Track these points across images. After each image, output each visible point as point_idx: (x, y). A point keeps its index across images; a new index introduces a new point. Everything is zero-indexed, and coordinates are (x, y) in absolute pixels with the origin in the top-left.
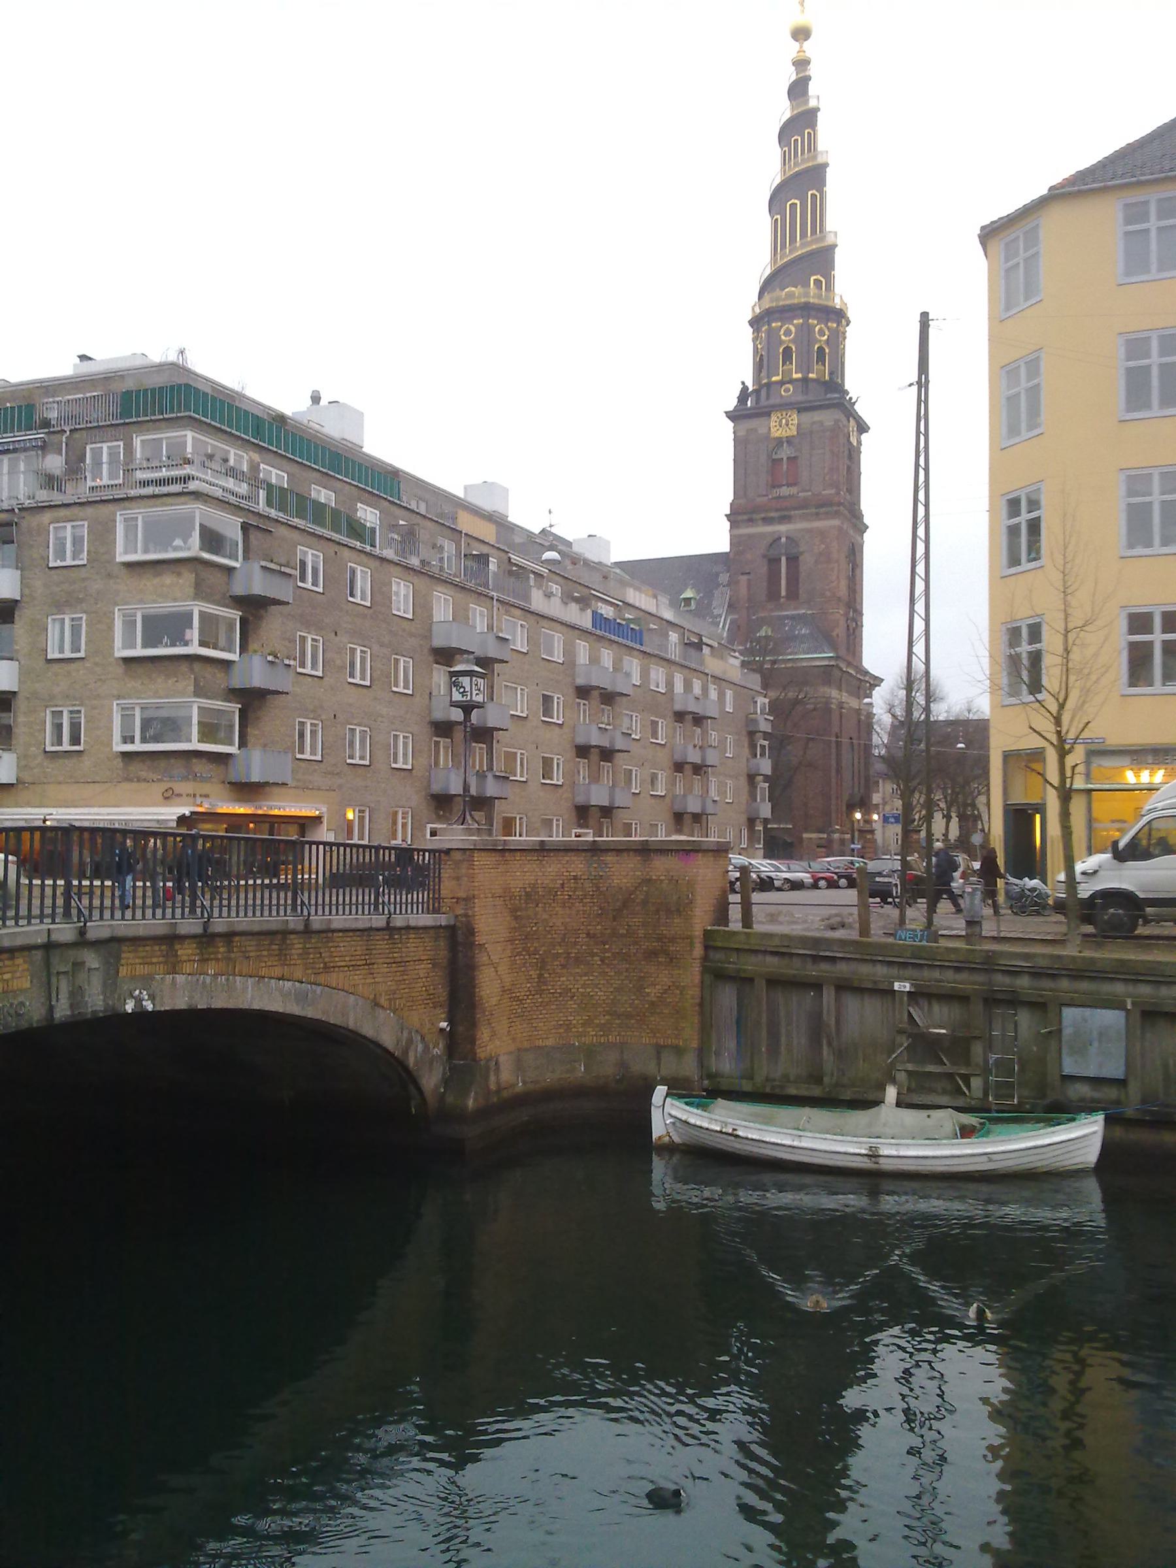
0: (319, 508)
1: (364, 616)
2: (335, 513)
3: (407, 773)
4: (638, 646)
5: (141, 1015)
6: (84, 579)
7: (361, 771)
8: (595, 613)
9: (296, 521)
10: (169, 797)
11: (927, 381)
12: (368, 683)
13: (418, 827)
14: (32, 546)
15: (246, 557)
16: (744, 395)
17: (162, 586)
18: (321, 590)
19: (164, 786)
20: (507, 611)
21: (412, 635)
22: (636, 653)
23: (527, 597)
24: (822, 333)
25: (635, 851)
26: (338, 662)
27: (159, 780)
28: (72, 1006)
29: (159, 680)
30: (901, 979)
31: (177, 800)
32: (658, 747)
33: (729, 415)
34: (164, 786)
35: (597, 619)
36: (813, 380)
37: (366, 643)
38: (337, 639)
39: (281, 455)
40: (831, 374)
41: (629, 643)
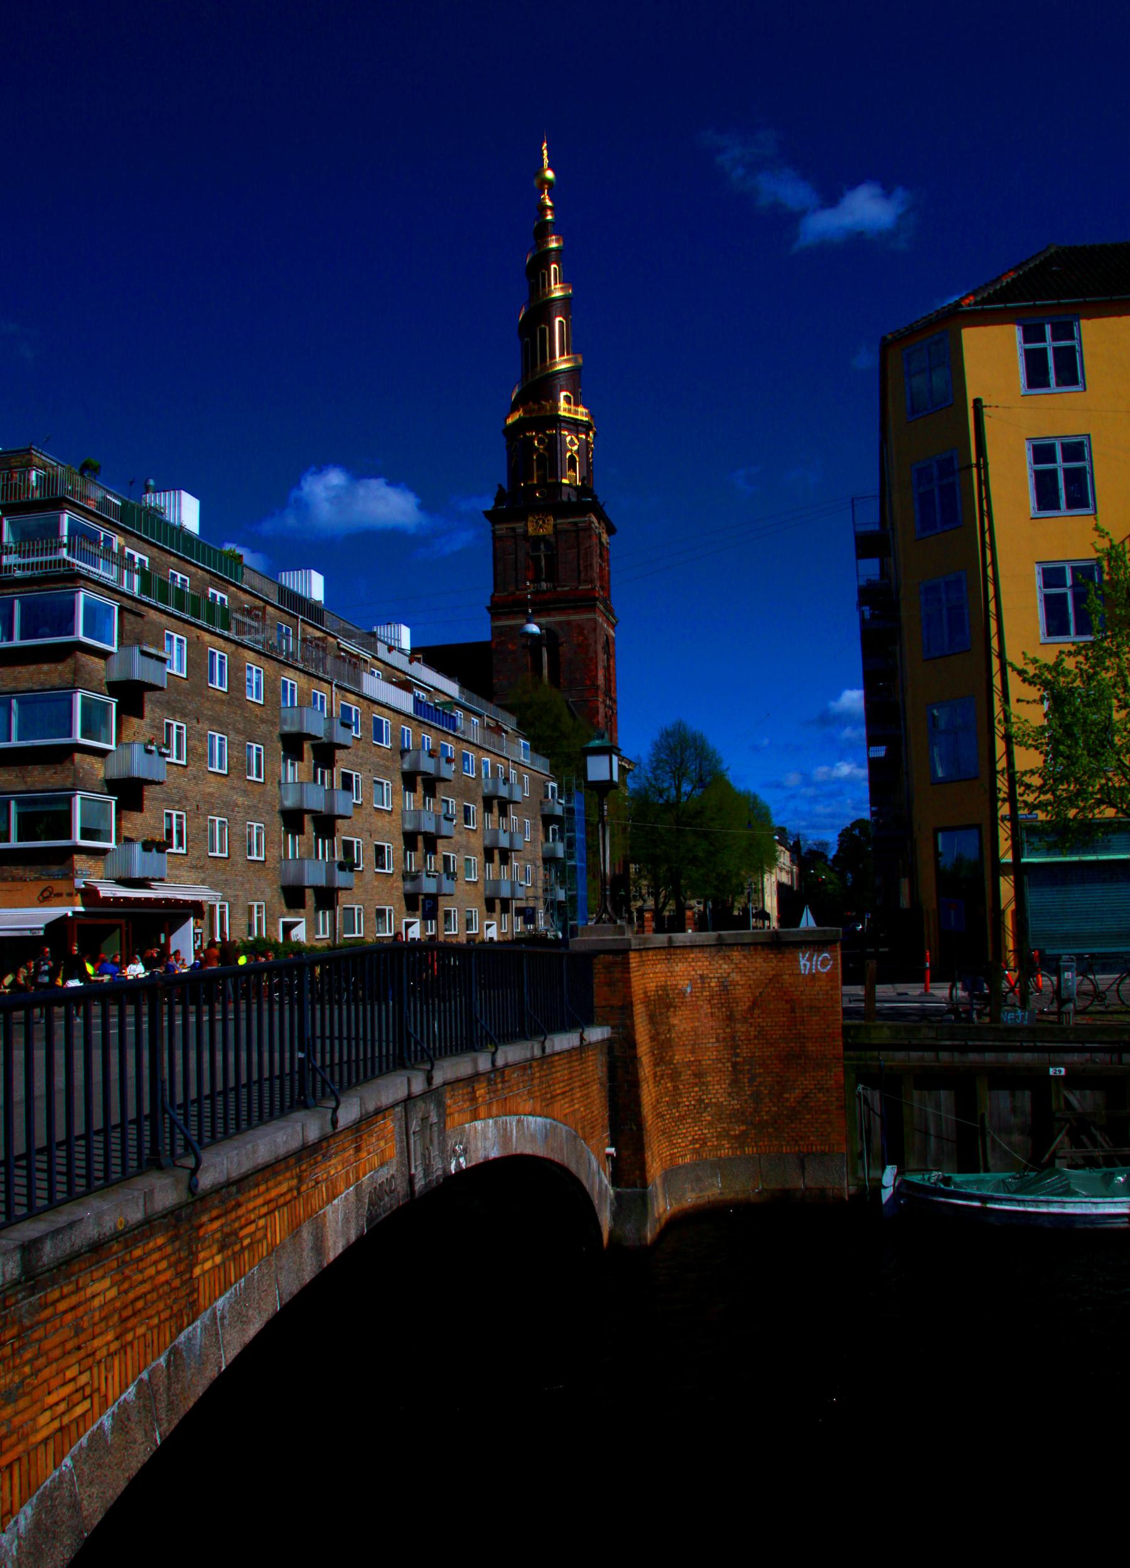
1: (222, 702)
3: (260, 865)
4: (451, 732)
5: (460, 1172)
7: (221, 864)
9: (161, 606)
10: (45, 899)
11: (986, 464)
12: (225, 772)
13: (272, 920)
15: (121, 644)
17: (39, 673)
19: (43, 885)
20: (344, 696)
21: (263, 721)
22: (450, 738)
23: (358, 682)
24: (572, 443)
25: (763, 944)
26: (200, 750)
27: (38, 879)
29: (36, 773)
30: (1055, 1065)
31: (54, 900)
32: (471, 834)
34: (43, 885)
37: (225, 730)
38: (200, 726)
40: (582, 480)
41: (445, 729)
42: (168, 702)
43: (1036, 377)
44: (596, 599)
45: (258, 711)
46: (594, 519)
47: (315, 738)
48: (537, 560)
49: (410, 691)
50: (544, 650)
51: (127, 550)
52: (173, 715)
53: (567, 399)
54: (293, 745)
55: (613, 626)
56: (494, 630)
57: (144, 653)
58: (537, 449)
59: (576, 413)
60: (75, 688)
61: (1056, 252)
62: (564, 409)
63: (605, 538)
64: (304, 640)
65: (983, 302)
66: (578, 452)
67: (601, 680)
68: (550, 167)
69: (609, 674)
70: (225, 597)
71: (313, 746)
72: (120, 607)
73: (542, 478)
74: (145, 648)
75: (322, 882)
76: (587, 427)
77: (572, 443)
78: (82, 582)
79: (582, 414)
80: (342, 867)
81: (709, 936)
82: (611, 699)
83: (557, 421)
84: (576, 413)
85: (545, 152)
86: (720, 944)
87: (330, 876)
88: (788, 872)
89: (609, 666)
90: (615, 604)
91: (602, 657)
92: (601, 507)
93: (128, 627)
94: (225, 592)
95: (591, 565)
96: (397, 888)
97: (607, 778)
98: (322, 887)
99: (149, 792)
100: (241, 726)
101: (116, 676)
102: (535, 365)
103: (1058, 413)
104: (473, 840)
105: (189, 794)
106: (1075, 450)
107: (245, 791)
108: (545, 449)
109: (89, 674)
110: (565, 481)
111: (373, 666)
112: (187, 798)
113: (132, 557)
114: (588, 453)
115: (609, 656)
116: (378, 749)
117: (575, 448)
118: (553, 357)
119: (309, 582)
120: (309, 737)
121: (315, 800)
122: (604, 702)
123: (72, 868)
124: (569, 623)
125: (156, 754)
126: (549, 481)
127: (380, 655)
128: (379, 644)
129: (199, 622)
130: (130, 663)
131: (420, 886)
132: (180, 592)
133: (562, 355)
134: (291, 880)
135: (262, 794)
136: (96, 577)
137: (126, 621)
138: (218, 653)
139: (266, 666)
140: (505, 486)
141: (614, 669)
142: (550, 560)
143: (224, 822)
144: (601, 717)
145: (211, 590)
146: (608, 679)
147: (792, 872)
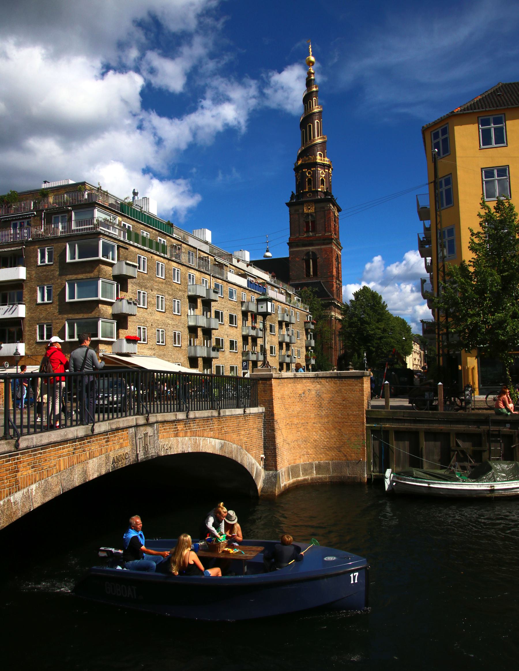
0: (144, 238)
1: (162, 283)
2: (151, 241)
6: (52, 270)
8: (248, 281)
9: (136, 244)
12: (164, 311)
14: (31, 257)
15: (118, 260)
16: (292, 197)
18: (146, 272)
21: (180, 290)
23: (222, 275)
26: (153, 302)
28: (144, 454)
33: (288, 204)
35: (249, 283)
36: (320, 191)
39: (511, 108)
40: (327, 189)
42: (139, 283)
43: (486, 140)
44: (333, 239)
45: (178, 286)
46: (331, 205)
47: (202, 297)
48: (307, 223)
49: (246, 278)
50: (311, 261)
51: (123, 222)
52: (141, 288)
53: (320, 155)
54: (193, 300)
55: (340, 250)
56: (291, 253)
57: (127, 264)
58: (308, 176)
59: (324, 160)
60: (99, 278)
61: (502, 86)
62: (319, 159)
63: (336, 214)
64: (199, 258)
65: (464, 110)
66: (325, 177)
67: (335, 273)
68: (312, 55)
69: (338, 270)
70: (165, 241)
71: (202, 301)
72: (118, 245)
73: (310, 188)
74: (128, 262)
75: (205, 355)
76: (329, 167)
77: (321, 173)
78: (101, 236)
79: (326, 161)
80: (214, 349)
81: (311, 374)
82: (339, 281)
83: (315, 164)
84: (324, 160)
85: (311, 50)
86: (317, 377)
87: (208, 353)
88: (418, 354)
89: (338, 267)
90: (341, 241)
91: (335, 263)
92: (335, 201)
93: (121, 253)
94: (165, 239)
95: (330, 225)
96: (239, 358)
97: (266, 311)
98: (205, 357)
99: (130, 319)
100: (171, 293)
101: (116, 273)
102: (306, 141)
103: (495, 157)
104: (273, 339)
105: (148, 320)
106: (503, 171)
107: (172, 319)
108: (311, 176)
109: (105, 272)
110: (319, 190)
111: (230, 268)
112: (147, 321)
113: (125, 225)
114: (329, 178)
115: (339, 263)
116: (231, 302)
117: (324, 176)
118: (314, 137)
119: (204, 234)
120: (200, 297)
121: (202, 322)
122: (336, 282)
123: (98, 349)
124: (321, 249)
125: (133, 304)
126: (313, 190)
127: (234, 264)
128: (233, 259)
129: (152, 251)
130: (121, 268)
131: (249, 357)
132: (143, 238)
133: (318, 136)
134: (192, 354)
135: (180, 320)
136: (107, 234)
137: (120, 251)
138: (161, 263)
139: (182, 269)
140: (295, 192)
141: (341, 268)
142: (313, 222)
143: (163, 331)
144: (335, 288)
145: (159, 238)
146: (338, 272)
147: (420, 353)
